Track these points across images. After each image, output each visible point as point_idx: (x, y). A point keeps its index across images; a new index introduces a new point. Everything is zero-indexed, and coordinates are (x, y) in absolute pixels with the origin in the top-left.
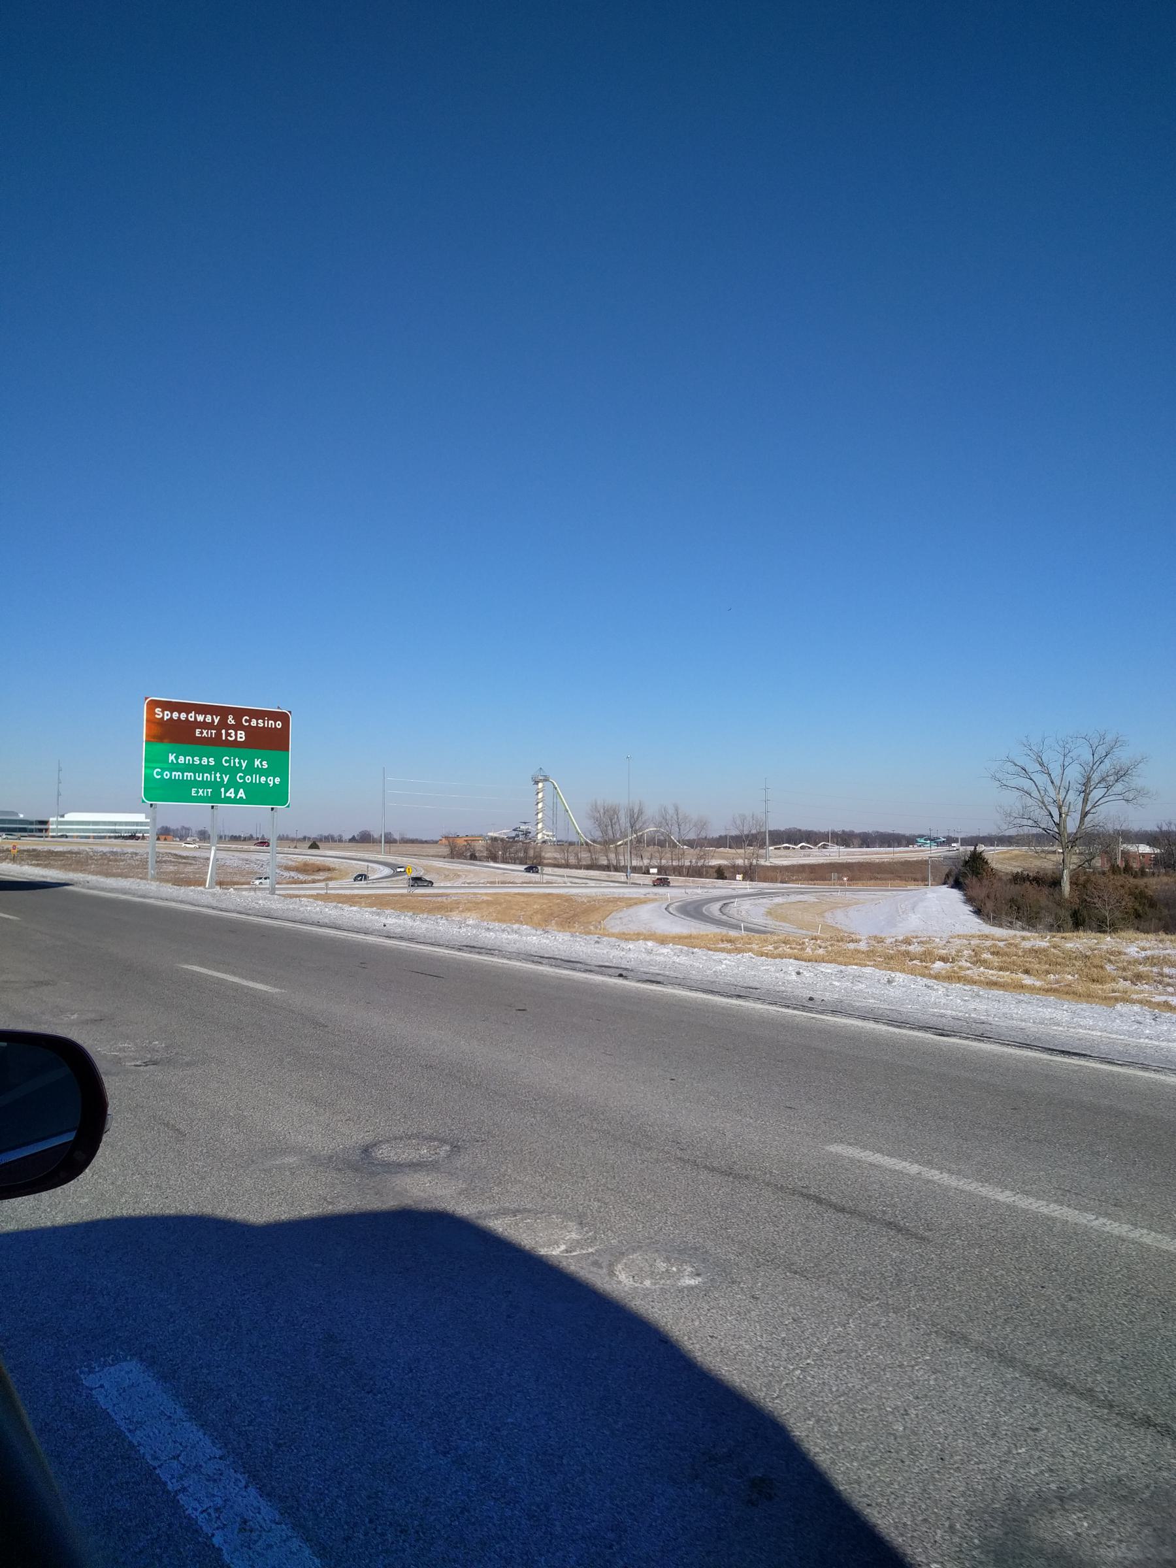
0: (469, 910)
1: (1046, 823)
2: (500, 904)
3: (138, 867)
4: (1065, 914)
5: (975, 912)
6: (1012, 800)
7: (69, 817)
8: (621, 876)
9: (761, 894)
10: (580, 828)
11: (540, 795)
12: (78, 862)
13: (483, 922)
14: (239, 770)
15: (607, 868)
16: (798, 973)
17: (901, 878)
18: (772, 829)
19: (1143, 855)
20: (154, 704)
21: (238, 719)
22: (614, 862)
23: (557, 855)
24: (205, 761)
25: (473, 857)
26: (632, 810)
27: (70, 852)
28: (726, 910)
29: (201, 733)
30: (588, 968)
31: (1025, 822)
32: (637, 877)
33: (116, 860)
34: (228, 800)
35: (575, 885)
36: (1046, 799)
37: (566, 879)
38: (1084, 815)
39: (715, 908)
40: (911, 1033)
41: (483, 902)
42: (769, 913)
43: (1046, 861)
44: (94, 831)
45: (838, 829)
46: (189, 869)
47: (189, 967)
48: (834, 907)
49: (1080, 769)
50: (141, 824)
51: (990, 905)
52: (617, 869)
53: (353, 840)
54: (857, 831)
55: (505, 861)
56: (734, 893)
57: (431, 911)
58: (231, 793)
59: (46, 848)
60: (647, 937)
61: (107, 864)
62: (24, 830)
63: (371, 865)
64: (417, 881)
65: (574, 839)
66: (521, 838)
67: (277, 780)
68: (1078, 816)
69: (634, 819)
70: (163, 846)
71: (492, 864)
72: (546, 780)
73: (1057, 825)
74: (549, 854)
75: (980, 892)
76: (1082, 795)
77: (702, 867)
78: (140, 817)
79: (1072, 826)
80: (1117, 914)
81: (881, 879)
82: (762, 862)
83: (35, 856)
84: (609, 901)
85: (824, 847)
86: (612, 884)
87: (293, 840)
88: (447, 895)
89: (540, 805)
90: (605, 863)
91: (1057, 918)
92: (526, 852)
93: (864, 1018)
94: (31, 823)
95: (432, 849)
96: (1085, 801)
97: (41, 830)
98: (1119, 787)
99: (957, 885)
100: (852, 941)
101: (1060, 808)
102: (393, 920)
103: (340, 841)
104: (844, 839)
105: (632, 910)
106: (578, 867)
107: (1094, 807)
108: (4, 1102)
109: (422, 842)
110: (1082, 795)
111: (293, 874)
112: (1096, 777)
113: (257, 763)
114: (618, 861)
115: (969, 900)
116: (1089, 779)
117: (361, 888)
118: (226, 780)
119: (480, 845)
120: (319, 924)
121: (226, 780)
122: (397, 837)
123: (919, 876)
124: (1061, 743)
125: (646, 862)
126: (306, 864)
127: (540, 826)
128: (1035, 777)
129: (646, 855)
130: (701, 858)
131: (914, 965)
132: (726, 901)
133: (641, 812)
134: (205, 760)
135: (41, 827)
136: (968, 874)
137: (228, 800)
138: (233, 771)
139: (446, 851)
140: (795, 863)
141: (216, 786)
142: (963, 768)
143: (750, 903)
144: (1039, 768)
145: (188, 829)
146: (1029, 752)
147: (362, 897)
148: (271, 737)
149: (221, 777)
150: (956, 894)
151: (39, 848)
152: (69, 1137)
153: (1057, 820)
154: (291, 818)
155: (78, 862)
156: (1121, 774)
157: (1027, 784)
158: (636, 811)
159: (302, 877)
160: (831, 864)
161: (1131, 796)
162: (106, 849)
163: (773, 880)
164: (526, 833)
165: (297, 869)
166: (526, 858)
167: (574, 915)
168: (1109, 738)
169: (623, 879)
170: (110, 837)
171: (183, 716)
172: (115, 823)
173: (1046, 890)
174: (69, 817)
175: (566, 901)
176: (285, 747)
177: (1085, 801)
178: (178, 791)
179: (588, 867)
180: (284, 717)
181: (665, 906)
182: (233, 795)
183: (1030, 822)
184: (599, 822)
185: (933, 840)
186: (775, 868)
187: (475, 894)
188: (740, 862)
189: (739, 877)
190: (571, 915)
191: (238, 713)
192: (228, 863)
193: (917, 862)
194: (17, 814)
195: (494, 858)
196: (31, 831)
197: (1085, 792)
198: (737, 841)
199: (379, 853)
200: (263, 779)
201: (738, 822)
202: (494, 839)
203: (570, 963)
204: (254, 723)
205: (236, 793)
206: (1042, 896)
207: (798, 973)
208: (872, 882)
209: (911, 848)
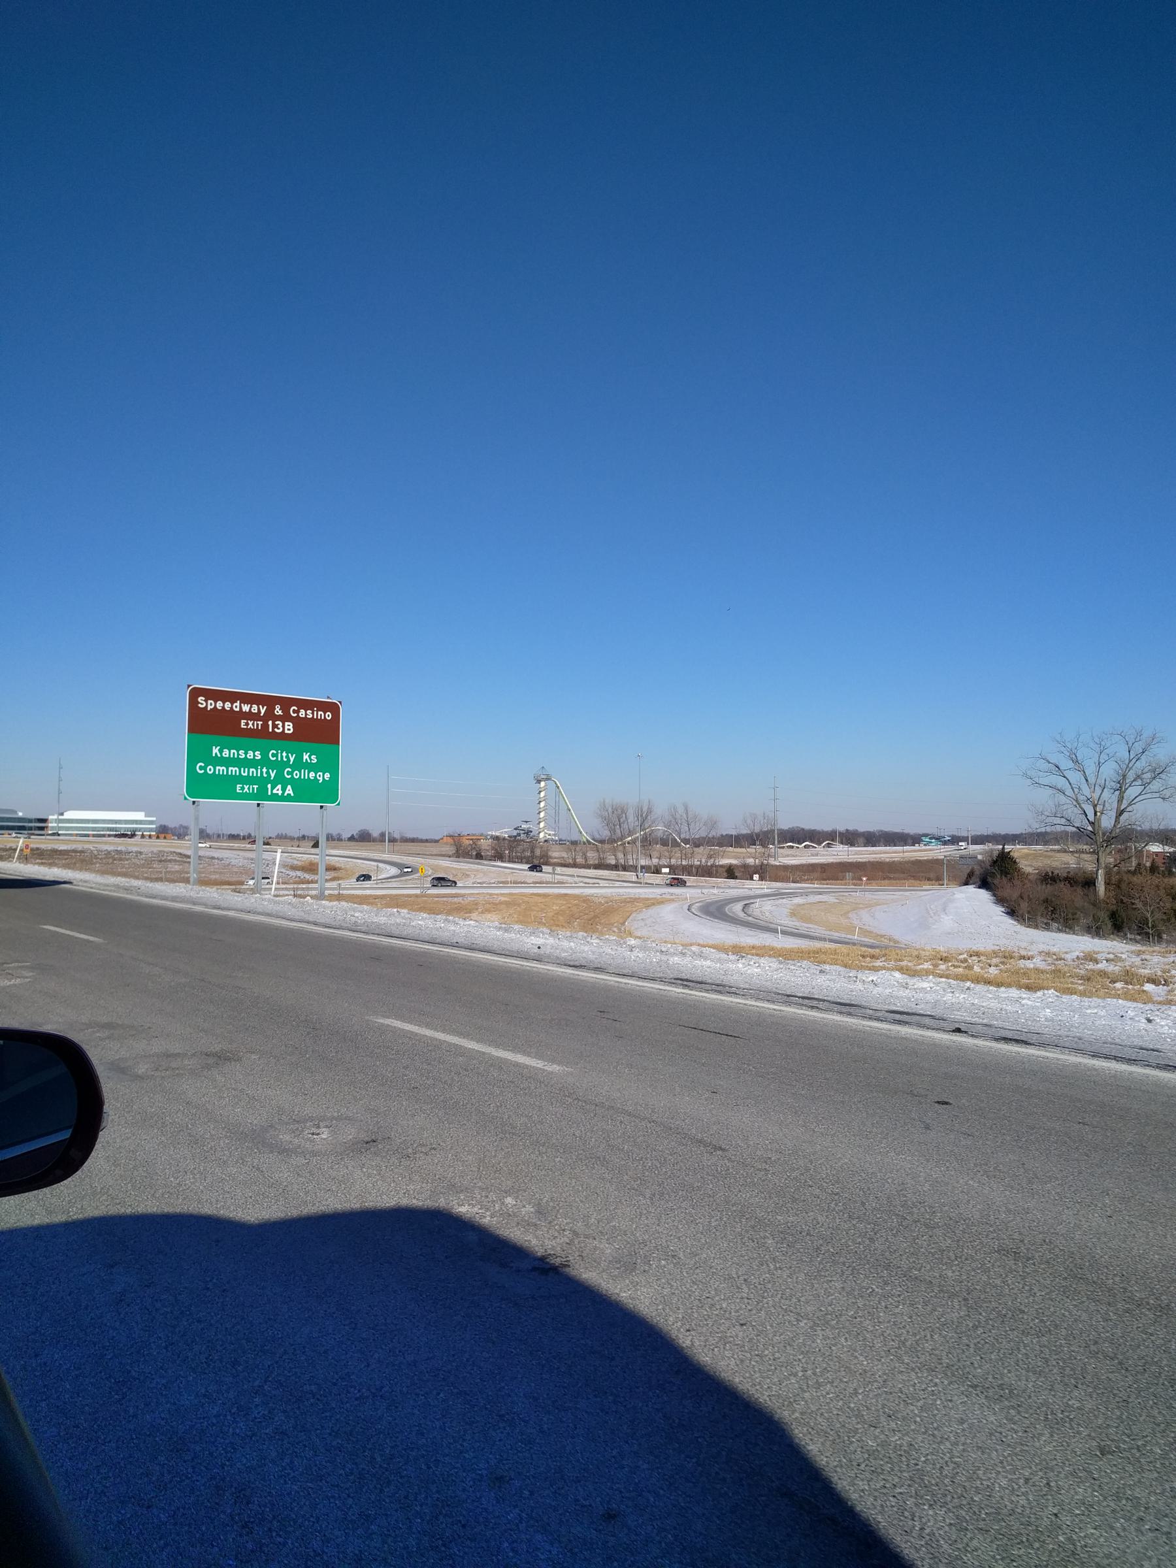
0: (488, 911)
1: (1079, 821)
2: (519, 905)
3: (143, 866)
4: (1103, 915)
5: (1007, 913)
6: (1044, 798)
7: (69, 815)
8: (631, 876)
9: (778, 895)
10: (585, 826)
11: (542, 794)
12: (82, 861)
13: (494, 923)
14: (287, 764)
15: (615, 867)
16: (1149, 1021)
17: (915, 878)
18: (785, 827)
19: (1157, 854)
20: (195, 693)
21: (285, 710)
22: (622, 861)
23: (565, 855)
24: (250, 755)
25: (479, 856)
27: (75, 851)
28: (750, 911)
29: (247, 724)
30: (844, 1009)
31: (1057, 820)
32: (649, 877)
33: (121, 859)
34: (275, 797)
35: (587, 885)
36: (1081, 798)
37: (576, 879)
38: (1120, 813)
39: (737, 908)
40: (1148, 1071)
41: (501, 903)
42: (793, 914)
43: (1065, 860)
44: (94, 829)
45: (841, 828)
47: (388, 1021)
48: (856, 908)
49: (1115, 766)
50: (141, 822)
51: (1024, 906)
52: (625, 868)
53: (352, 839)
54: (861, 829)
55: (511, 861)
56: (751, 893)
57: (449, 913)
58: (278, 790)
59: (50, 846)
60: (672, 938)
61: (110, 863)
62: (23, 828)
63: (381, 865)
64: (440, 881)
65: (575, 837)
66: (523, 836)
67: (327, 776)
68: (1113, 814)
69: (644, 817)
70: (163, 845)
71: (499, 864)
72: (547, 779)
73: (1092, 824)
74: (556, 854)
75: (1011, 892)
76: (1117, 793)
77: (712, 866)
78: (140, 816)
79: (1107, 822)
80: (1159, 915)
81: (895, 879)
82: (772, 862)
83: (38, 855)
84: (625, 901)
85: (829, 845)
87: (292, 839)
88: (463, 896)
89: (542, 804)
90: (613, 862)
91: (1096, 919)
92: (532, 852)
94: (30, 821)
95: (434, 849)
96: (1120, 800)
97: (42, 828)
98: (1156, 785)
99: (984, 884)
100: (1023, 958)
101: (1095, 806)
102: (423, 923)
103: (340, 839)
104: (850, 838)
105: (652, 911)
106: (588, 867)
107: (1130, 805)
108: (3, 1099)
109: (422, 841)
110: (1117, 793)
111: (299, 873)
112: (1131, 775)
113: (306, 757)
114: (626, 860)
115: (1000, 900)
116: (1124, 776)
117: (366, 889)
118: (273, 776)
119: (485, 844)
120: (456, 945)
121: (273, 776)
122: (397, 836)
123: (932, 875)
124: (1097, 740)
125: (655, 861)
127: (542, 825)
128: (1067, 773)
129: (655, 854)
130: (710, 857)
131: (951, 965)
132: (747, 902)
133: (650, 811)
134: (251, 753)
135: (39, 825)
136: (995, 874)
137: (275, 797)
138: (280, 766)
139: (451, 850)
140: (804, 862)
141: (262, 782)
142: (999, 767)
143: (774, 903)
144: (1071, 765)
146: (1063, 749)
147: (376, 897)
148: (320, 729)
149: (268, 773)
150: (984, 895)
151: (43, 846)
152: (66, 1135)
153: (1091, 818)
154: (344, 814)
155: (82, 861)
156: (1158, 772)
157: (1061, 782)
158: (645, 809)
160: (840, 863)
161: (1167, 793)
162: (111, 848)
163: (785, 880)
164: (528, 832)
165: (303, 869)
166: (533, 857)
167: (595, 917)
168: (1147, 734)
169: (634, 879)
170: (109, 836)
171: (228, 706)
172: (116, 822)
173: (1079, 890)
174: (69, 815)
175: (584, 901)
176: (336, 741)
177: (1120, 800)
178: (223, 788)
179: (597, 867)
180: (333, 708)
181: (686, 907)
182: (280, 792)
183: (1063, 821)
184: (608, 822)
185: (938, 839)
186: (786, 868)
187: (491, 895)
188: (751, 861)
189: (756, 877)
190: (594, 917)
191: (286, 703)
192: (234, 862)
193: (928, 861)
194: (15, 812)
195: (499, 857)
196: (31, 829)
197: (1121, 789)
198: (751, 839)
199: (383, 852)
200: (312, 775)
201: (749, 821)
202: (497, 838)
203: (809, 1001)
204: (302, 713)
205: (284, 790)
206: (1077, 897)
207: (1149, 1021)
208: (887, 881)
209: (917, 847)
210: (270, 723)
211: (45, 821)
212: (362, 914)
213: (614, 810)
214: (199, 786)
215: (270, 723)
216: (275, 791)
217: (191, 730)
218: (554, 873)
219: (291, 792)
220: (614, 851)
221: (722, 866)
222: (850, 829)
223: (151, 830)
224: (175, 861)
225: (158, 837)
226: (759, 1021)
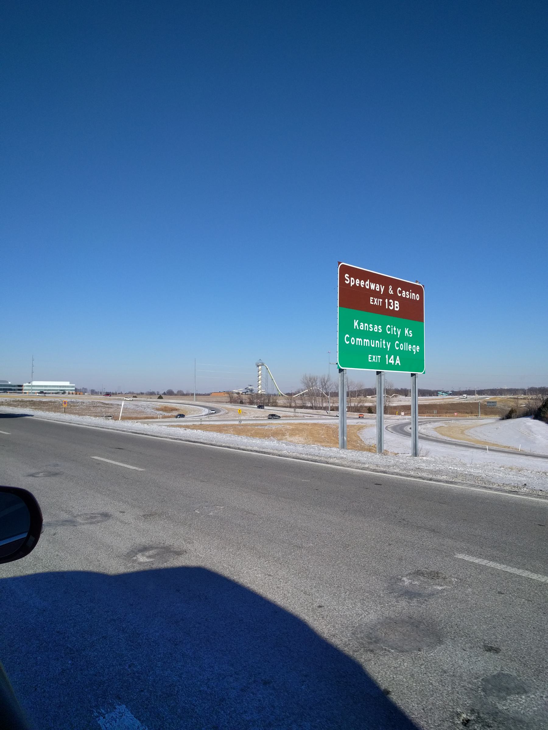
7: (35, 383)
11: (260, 372)
12: (55, 407)
15: (311, 408)
20: (344, 270)
25: (241, 403)
26: (324, 379)
33: (74, 406)
46: (111, 410)
47: (134, 468)
50: (68, 387)
69: (324, 383)
72: (263, 365)
78: (67, 383)
86: (329, 417)
89: (260, 377)
93: (392, 474)
94: (15, 386)
97: (21, 390)
111: (161, 412)
122: (175, 392)
126: (165, 407)
127: (260, 387)
135: (19, 388)
138: (391, 338)
145: (86, 389)
152: (25, 535)
155: (55, 407)
158: (326, 379)
159: (166, 414)
169: (326, 414)
170: (53, 393)
174: (35, 383)
176: (420, 318)
182: (393, 362)
185: (446, 393)
191: (396, 284)
194: (7, 382)
196: (15, 390)
199: (193, 400)
210: (386, 300)
211: (21, 386)
212: (181, 432)
213: (310, 379)
214: (351, 356)
215: (386, 300)
216: (390, 361)
217: (342, 304)
218: (295, 412)
219: (399, 362)
220: (310, 400)
221: (366, 407)
222: (403, 388)
223: (72, 390)
224: (101, 406)
225: (76, 394)
226: (172, 444)
